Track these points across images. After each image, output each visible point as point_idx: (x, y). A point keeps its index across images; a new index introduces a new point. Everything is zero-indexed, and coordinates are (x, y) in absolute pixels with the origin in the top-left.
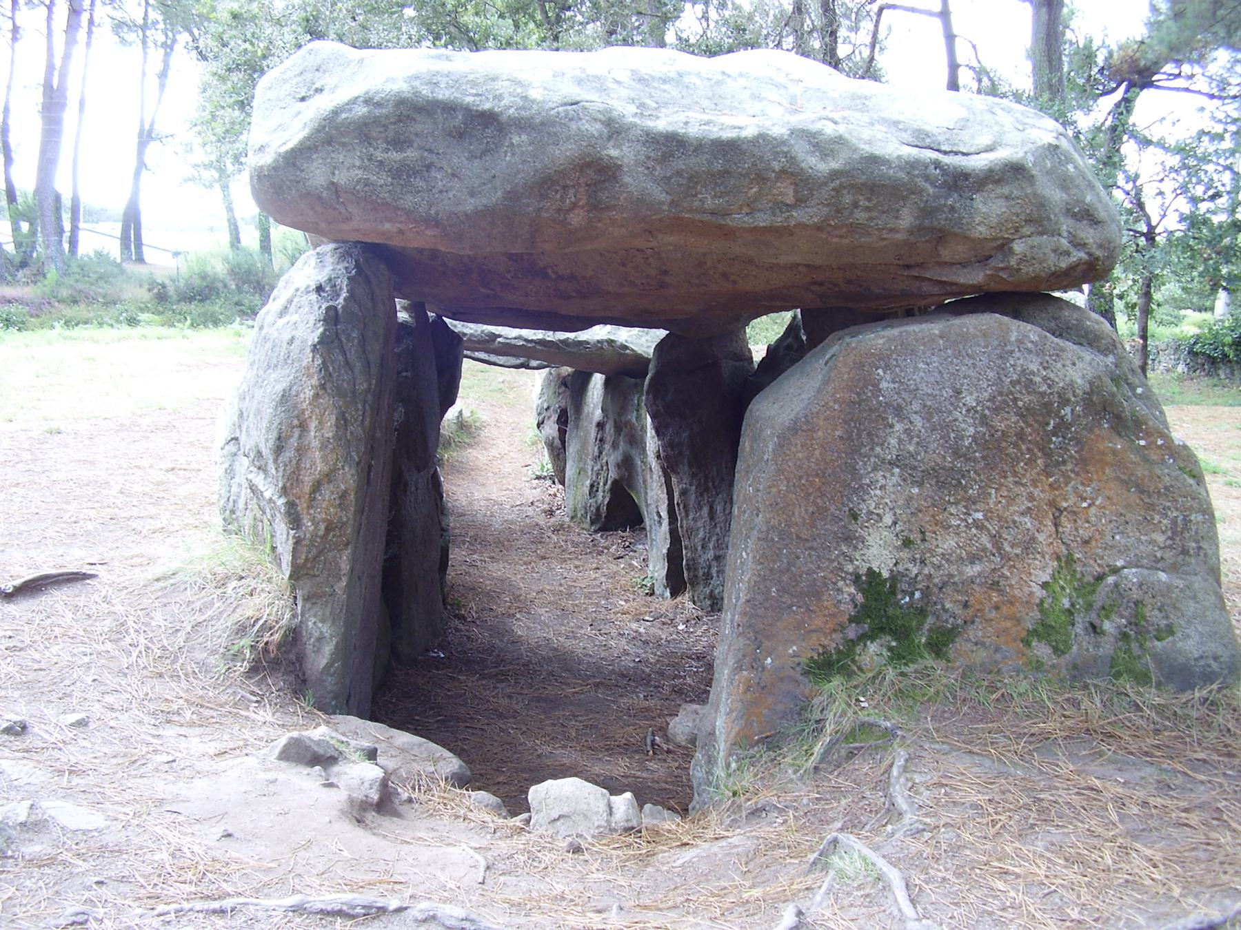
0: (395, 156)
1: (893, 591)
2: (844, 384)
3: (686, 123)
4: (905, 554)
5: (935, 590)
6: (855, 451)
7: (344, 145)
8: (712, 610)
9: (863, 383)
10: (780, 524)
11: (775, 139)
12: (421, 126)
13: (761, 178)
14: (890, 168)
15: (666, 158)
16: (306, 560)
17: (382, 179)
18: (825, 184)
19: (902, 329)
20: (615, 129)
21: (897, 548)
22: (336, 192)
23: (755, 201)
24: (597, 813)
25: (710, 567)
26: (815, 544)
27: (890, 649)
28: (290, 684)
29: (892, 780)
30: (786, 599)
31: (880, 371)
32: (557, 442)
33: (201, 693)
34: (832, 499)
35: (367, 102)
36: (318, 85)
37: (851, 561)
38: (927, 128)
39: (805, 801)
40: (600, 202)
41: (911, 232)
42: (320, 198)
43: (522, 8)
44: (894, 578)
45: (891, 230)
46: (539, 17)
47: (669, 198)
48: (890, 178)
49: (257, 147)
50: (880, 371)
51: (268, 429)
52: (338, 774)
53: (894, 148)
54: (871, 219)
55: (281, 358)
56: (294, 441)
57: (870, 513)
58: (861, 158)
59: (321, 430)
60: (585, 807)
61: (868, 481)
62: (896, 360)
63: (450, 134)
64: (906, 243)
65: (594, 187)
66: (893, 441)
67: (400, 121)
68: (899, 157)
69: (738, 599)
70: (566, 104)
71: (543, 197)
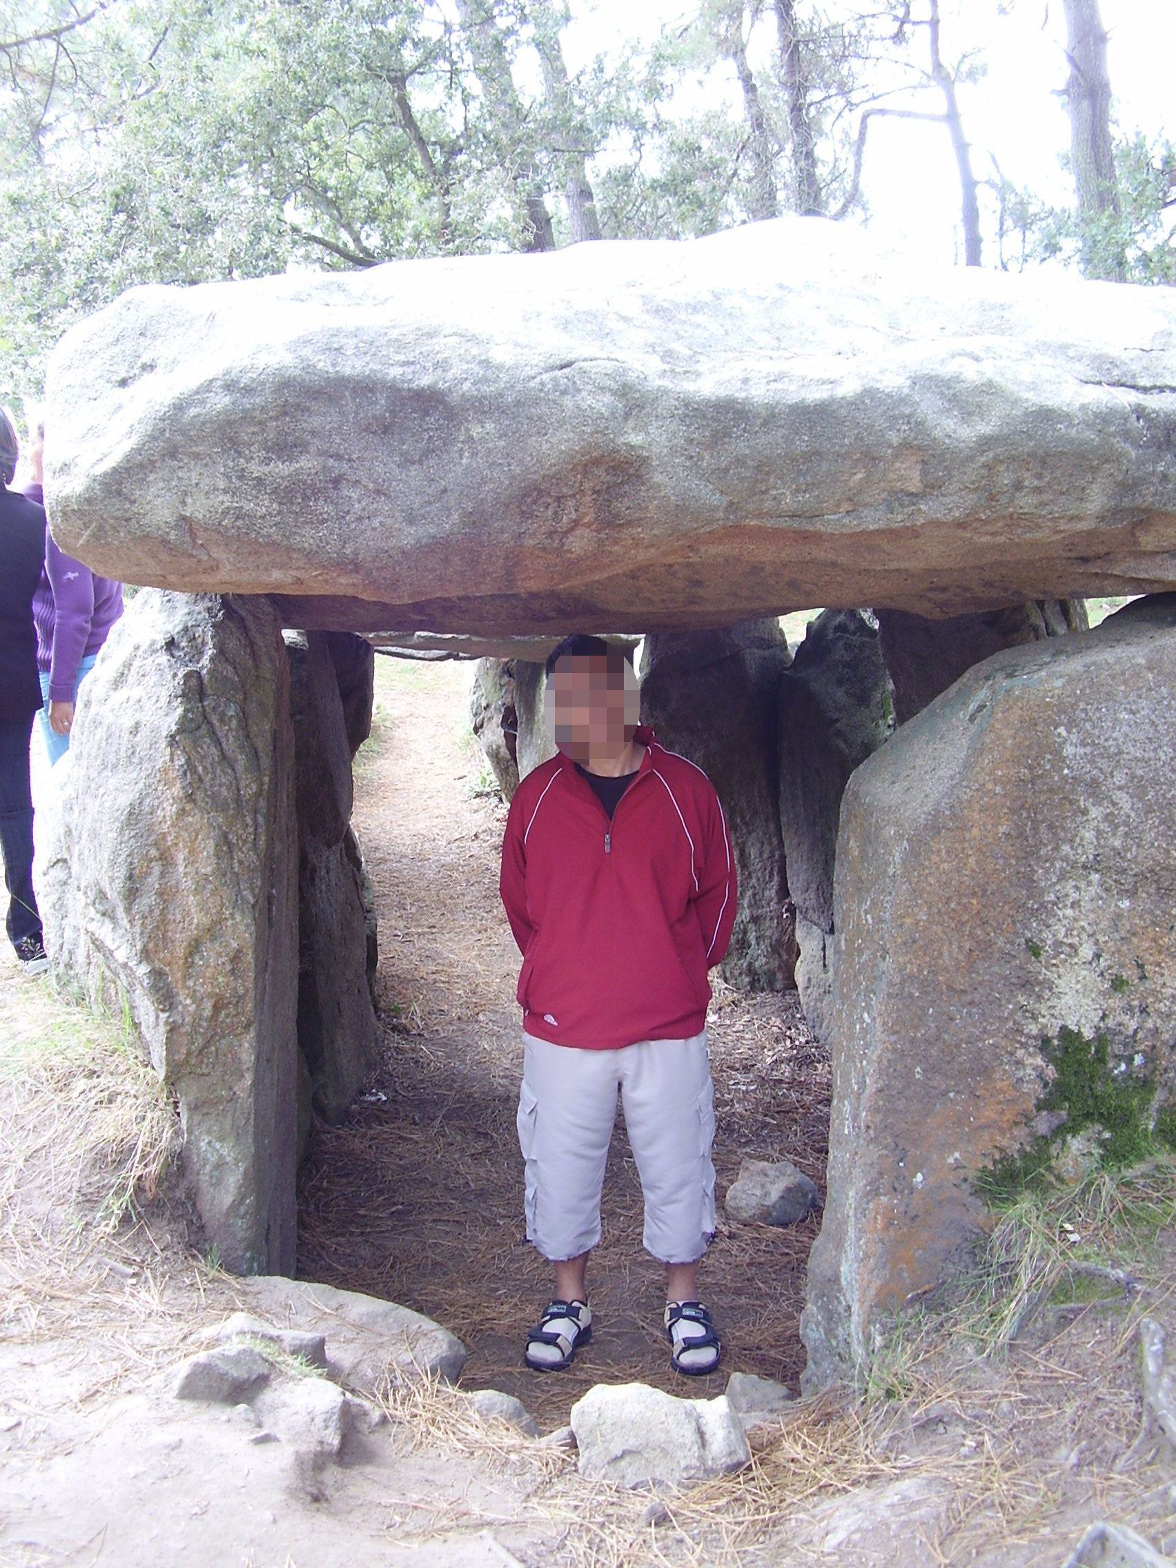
0: (281, 469)
1: (1101, 1059)
2: (1008, 754)
3: (746, 381)
4: (1116, 1002)
5: (1165, 1050)
6: (1030, 854)
7: (197, 456)
8: (753, 989)
9: (1036, 750)
10: (920, 971)
11: (889, 396)
12: (320, 419)
13: (870, 458)
14: (1071, 425)
15: (718, 439)
16: (189, 1054)
17: (263, 506)
18: (971, 459)
19: (1088, 660)
20: (634, 401)
21: (1103, 994)
22: (191, 530)
23: (860, 491)
24: (682, 1446)
25: (745, 932)
26: (977, 997)
27: (1103, 1144)
28: (181, 1235)
29: (1149, 1380)
30: (938, 1082)
31: (1062, 730)
32: (504, 752)
33: (48, 1272)
34: (1000, 929)
35: (229, 387)
36: (145, 359)
37: (1034, 1018)
38: (1114, 352)
39: (1005, 1405)
40: (617, 516)
41: (1102, 518)
42: (165, 542)
43: (396, 155)
44: (1102, 1039)
45: (1071, 519)
46: (419, 165)
47: (725, 500)
48: (1072, 441)
49: (58, 466)
50: (1062, 730)
51: (113, 863)
52: (274, 1408)
53: (1071, 393)
54: (1043, 504)
55: (123, 754)
56: (153, 881)
57: (1058, 944)
58: (1025, 414)
59: (195, 864)
60: (663, 1437)
61: (1052, 897)
62: (1084, 710)
63: (367, 429)
64: (1090, 534)
65: (606, 495)
66: (1089, 835)
67: (285, 414)
68: (1083, 407)
69: (862, 1085)
70: (552, 368)
71: (525, 515)
